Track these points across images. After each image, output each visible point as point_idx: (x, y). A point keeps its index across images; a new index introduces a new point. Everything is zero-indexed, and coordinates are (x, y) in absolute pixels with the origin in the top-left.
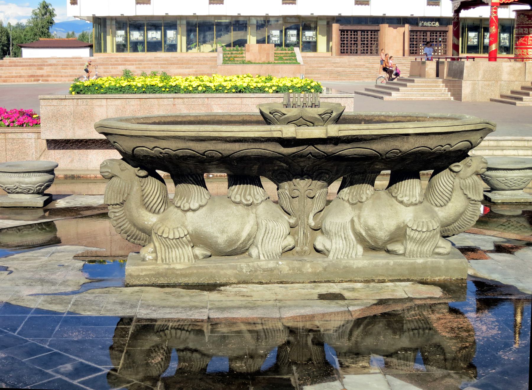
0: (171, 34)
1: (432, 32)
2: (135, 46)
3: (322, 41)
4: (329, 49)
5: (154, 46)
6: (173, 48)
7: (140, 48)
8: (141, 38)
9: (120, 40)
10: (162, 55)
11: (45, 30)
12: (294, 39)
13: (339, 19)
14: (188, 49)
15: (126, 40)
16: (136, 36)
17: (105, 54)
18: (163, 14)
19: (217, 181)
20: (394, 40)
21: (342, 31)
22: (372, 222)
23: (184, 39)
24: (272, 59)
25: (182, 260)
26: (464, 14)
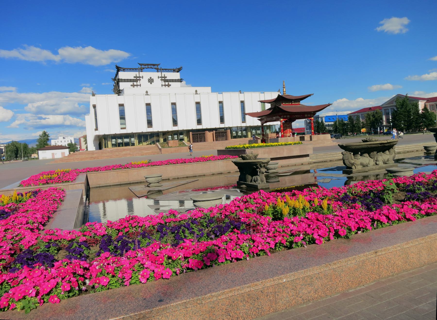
0: (133, 139)
1: (222, 133)
2: (119, 145)
3: (186, 138)
4: (189, 141)
5: (127, 144)
6: (133, 144)
7: (121, 145)
8: (122, 142)
9: (114, 143)
10: (130, 147)
11: (45, 143)
12: (176, 138)
13: (192, 131)
14: (139, 144)
15: (116, 143)
16: (120, 141)
17: (107, 149)
18: (256, 125)
19: (171, 178)
20: (209, 135)
21: (193, 134)
22: (385, 158)
23: (137, 141)
24: (178, 145)
25: (360, 168)
26: (265, 124)
